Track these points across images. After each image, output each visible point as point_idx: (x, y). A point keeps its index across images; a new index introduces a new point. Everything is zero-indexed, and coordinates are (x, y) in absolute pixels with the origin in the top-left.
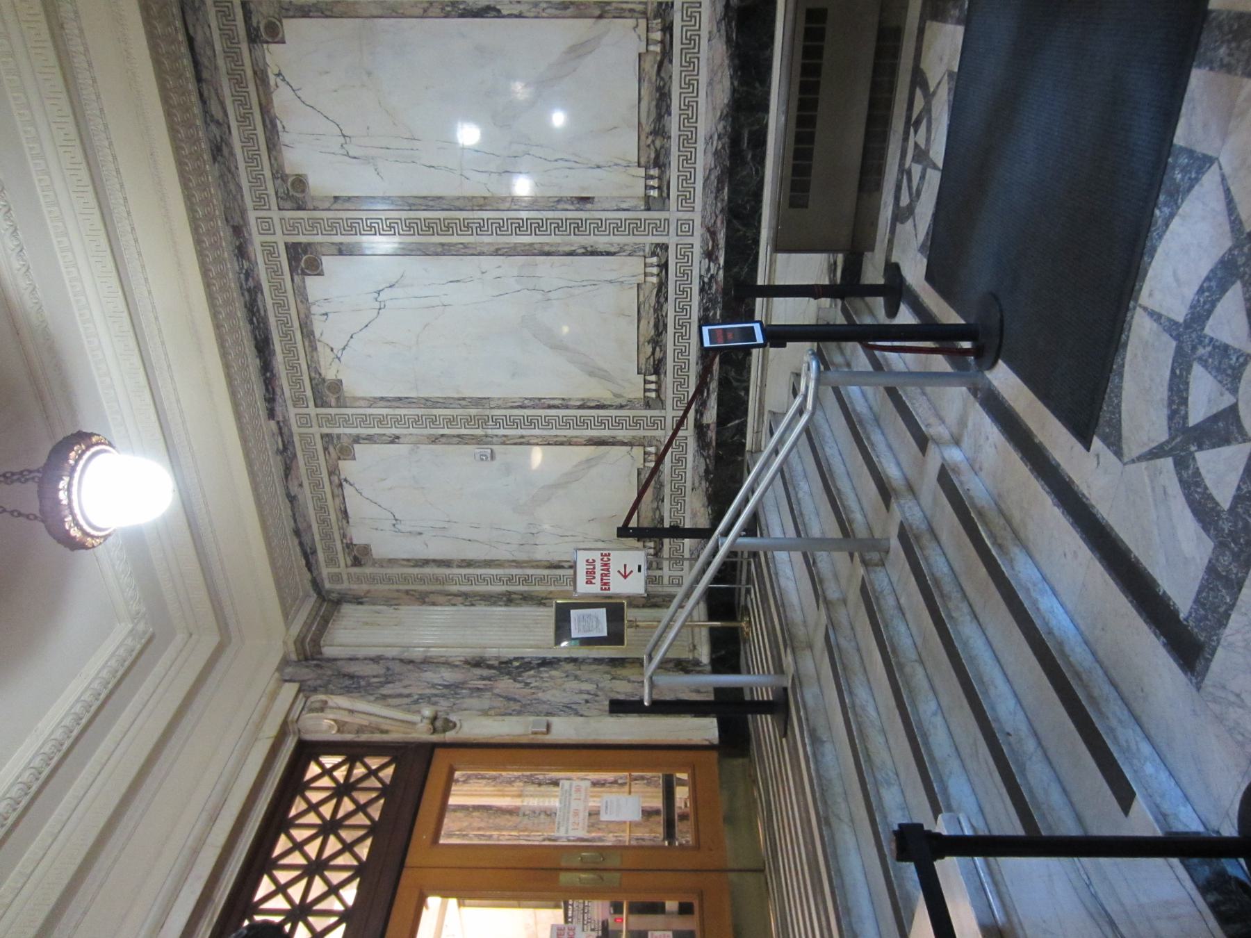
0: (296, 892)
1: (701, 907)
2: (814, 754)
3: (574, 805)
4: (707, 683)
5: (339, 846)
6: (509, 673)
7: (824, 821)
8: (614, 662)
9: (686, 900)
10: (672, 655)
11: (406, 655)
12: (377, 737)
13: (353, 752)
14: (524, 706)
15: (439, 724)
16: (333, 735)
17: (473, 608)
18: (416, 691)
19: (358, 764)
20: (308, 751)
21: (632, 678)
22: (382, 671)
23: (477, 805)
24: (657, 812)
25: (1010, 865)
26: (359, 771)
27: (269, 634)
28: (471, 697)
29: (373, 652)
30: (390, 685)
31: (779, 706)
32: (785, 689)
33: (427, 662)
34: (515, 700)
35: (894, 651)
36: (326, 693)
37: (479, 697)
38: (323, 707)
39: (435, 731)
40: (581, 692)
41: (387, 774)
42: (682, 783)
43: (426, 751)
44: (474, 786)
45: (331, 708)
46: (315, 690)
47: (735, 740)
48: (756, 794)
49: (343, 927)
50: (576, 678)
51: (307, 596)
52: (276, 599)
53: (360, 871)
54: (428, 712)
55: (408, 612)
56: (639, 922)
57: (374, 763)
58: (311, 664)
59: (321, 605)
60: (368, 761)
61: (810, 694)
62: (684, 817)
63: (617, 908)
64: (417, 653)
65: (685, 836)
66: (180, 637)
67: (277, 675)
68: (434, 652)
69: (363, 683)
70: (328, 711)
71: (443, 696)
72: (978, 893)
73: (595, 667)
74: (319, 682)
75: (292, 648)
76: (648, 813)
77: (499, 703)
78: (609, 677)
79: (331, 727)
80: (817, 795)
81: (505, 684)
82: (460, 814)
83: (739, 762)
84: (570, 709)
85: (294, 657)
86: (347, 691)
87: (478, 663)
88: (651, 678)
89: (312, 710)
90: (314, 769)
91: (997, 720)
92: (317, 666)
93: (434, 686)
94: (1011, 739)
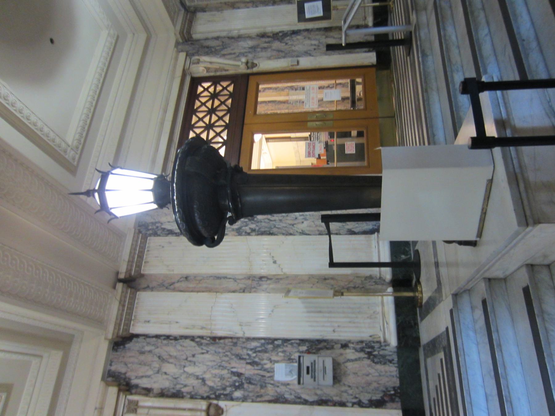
0: (207, 120)
1: (367, 133)
2: (423, 61)
3: (312, 95)
4: (371, 31)
5: (217, 118)
6: (278, 39)
7: (425, 91)
8: (327, 29)
9: (360, 130)
10: (353, 23)
11: (230, 35)
12: (224, 73)
13: (215, 80)
14: (286, 54)
15: (249, 65)
16: (205, 74)
17: (257, 9)
18: (237, 51)
19: (218, 85)
20: (196, 81)
21: (336, 36)
22: (221, 44)
23: (270, 97)
24: (347, 98)
25: (513, 94)
26: (219, 88)
27: (167, 32)
28: (262, 51)
29: (216, 35)
30: (226, 50)
31: (407, 42)
32: (411, 32)
33: (240, 38)
34: (282, 51)
35: (470, 4)
36: (198, 55)
37: (265, 51)
38: (198, 62)
39: (248, 68)
40: (312, 45)
41: (231, 88)
42: (359, 83)
43: (246, 77)
44: (268, 92)
45: (202, 62)
46: (193, 55)
47: (384, 62)
48: (393, 85)
49: (224, 147)
50: (309, 38)
51: (180, 10)
52: (166, 12)
53: (227, 127)
54: (244, 60)
55: (228, 13)
56: (340, 141)
57: (225, 84)
58: (188, 42)
59: (187, 14)
60: (222, 83)
61: (423, 33)
62: (360, 99)
63: (331, 135)
64: (235, 33)
65: (360, 106)
66: (130, 36)
67: (175, 49)
68: (242, 32)
69: (213, 50)
70: (200, 63)
71: (249, 52)
72: (496, 105)
73: (317, 33)
74: (194, 51)
75: (179, 36)
76: (344, 99)
77: (274, 53)
78: (324, 37)
79: (203, 70)
80: (423, 79)
81: (276, 45)
82: (263, 105)
83: (385, 72)
84: (307, 53)
85: (181, 41)
86: (207, 54)
87: (263, 35)
88: (345, 32)
89: (194, 63)
90: (200, 89)
91: (519, 33)
92: (192, 44)
93: (245, 48)
94: (525, 43)
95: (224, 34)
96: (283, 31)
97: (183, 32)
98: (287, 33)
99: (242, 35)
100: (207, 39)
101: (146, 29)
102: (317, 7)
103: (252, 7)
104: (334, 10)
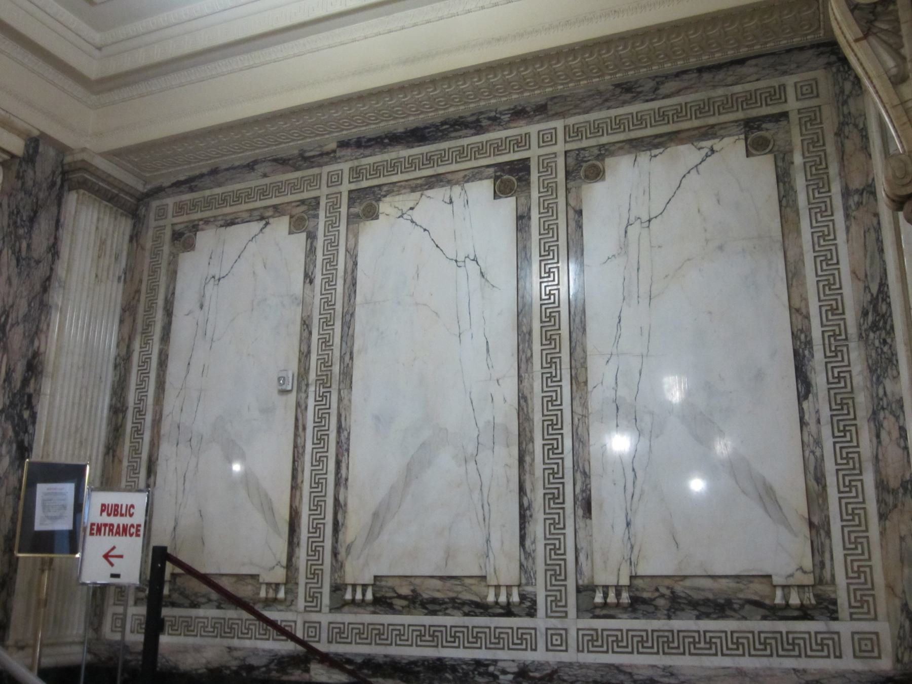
6: (12, 405)
11: (55, 284)
51: (146, 183)
59: (132, 196)
69: (21, 231)
74: (30, 183)
75: (79, 157)
85: (68, 159)
92: (53, 184)
95: (61, 269)
96: (34, 423)
97: (86, 170)
98: (26, 431)
99: (48, 313)
100: (58, 224)
101: (102, 81)
102: (61, 517)
103: (118, 355)
104: (254, 604)
